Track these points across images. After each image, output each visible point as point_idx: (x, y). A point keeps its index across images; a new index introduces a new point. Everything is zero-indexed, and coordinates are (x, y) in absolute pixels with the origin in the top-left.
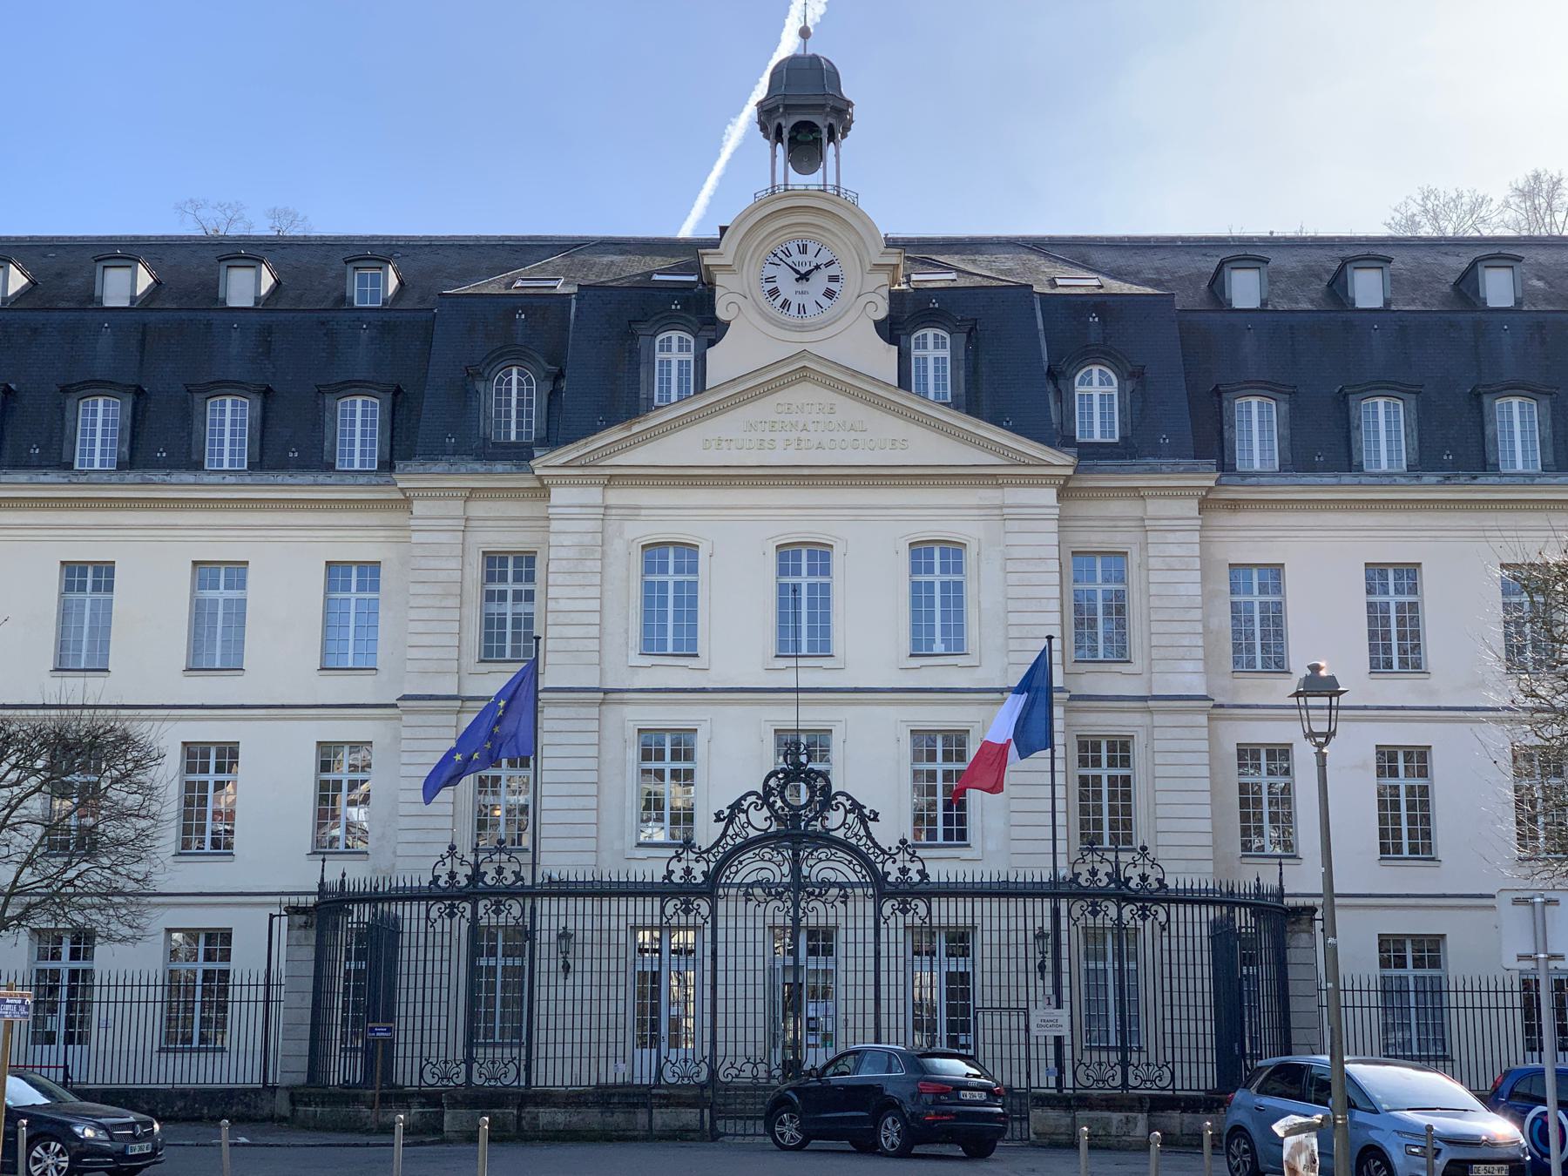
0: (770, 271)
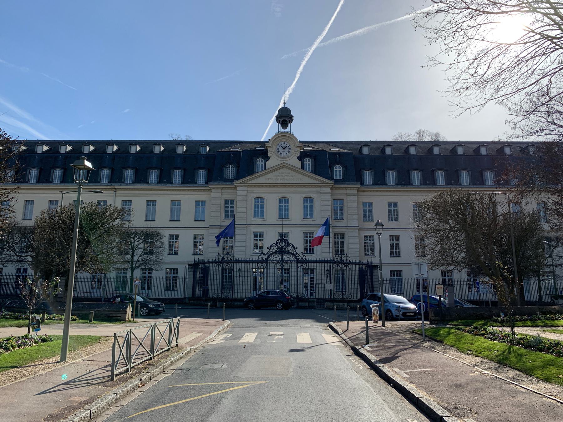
0: (278, 147)
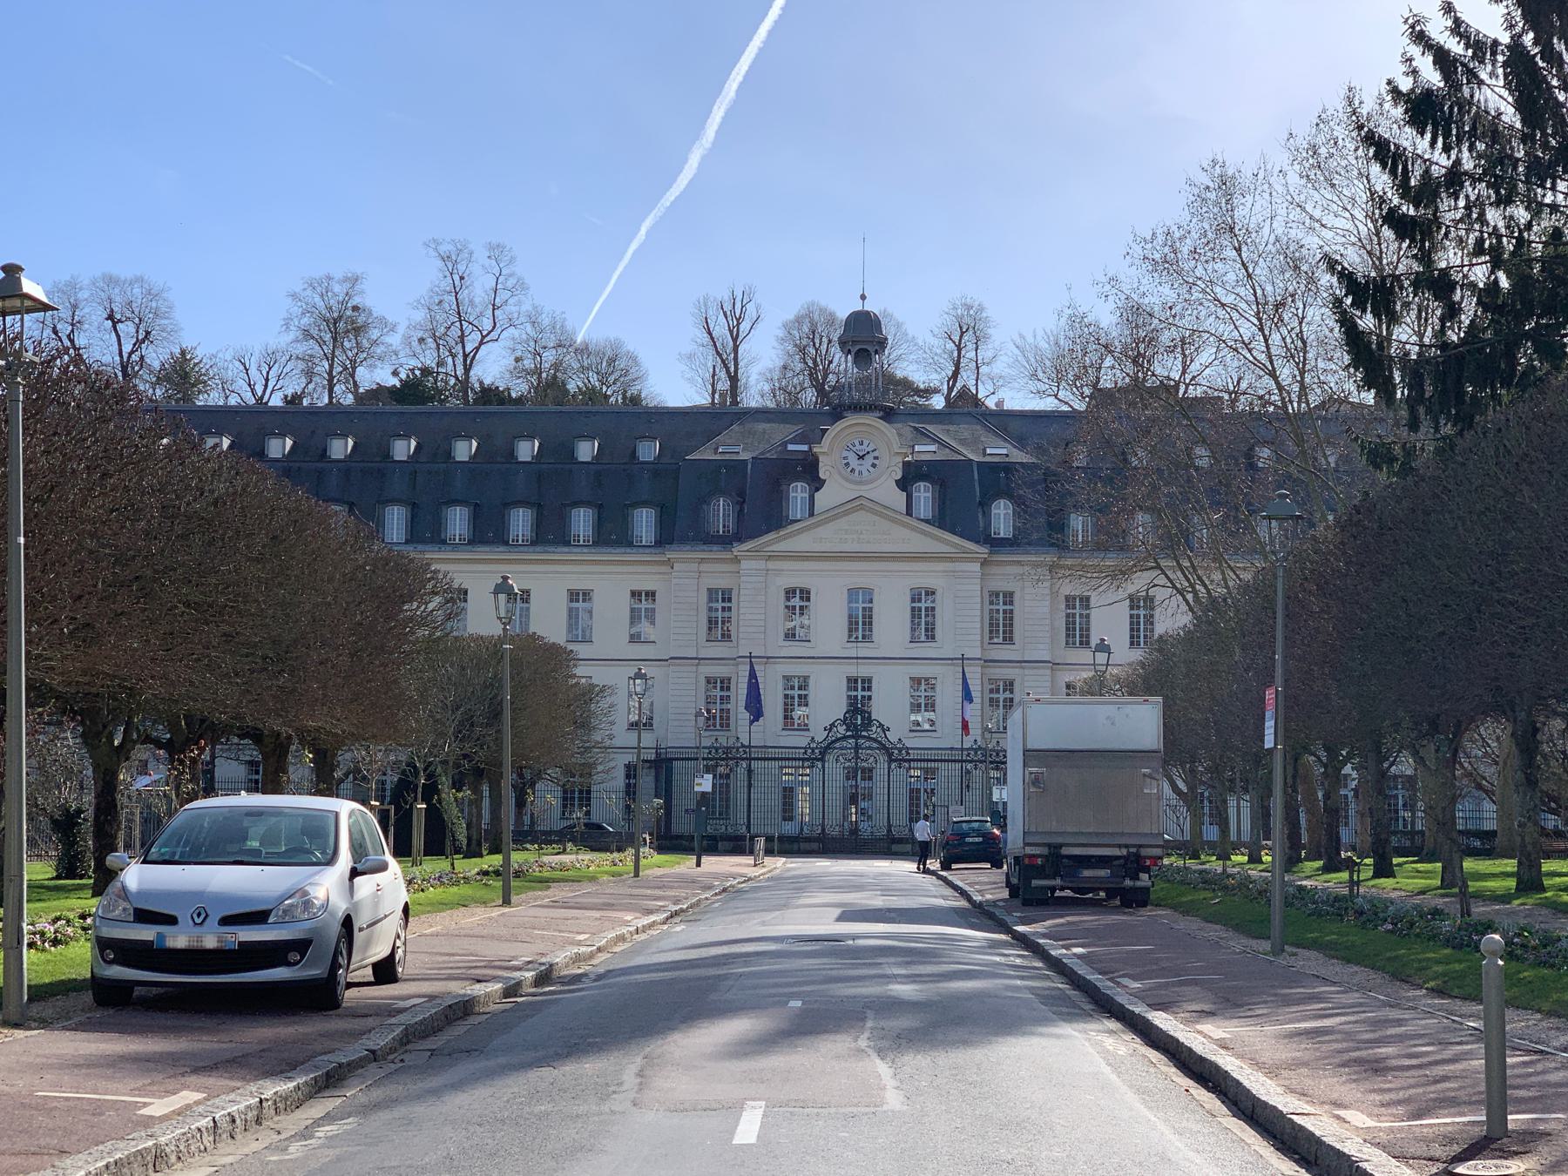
0: (845, 454)
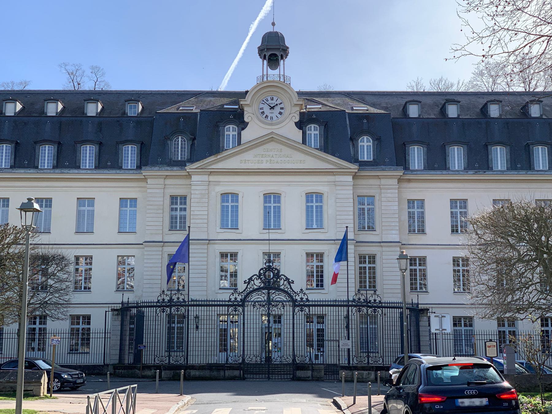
0: (262, 106)
